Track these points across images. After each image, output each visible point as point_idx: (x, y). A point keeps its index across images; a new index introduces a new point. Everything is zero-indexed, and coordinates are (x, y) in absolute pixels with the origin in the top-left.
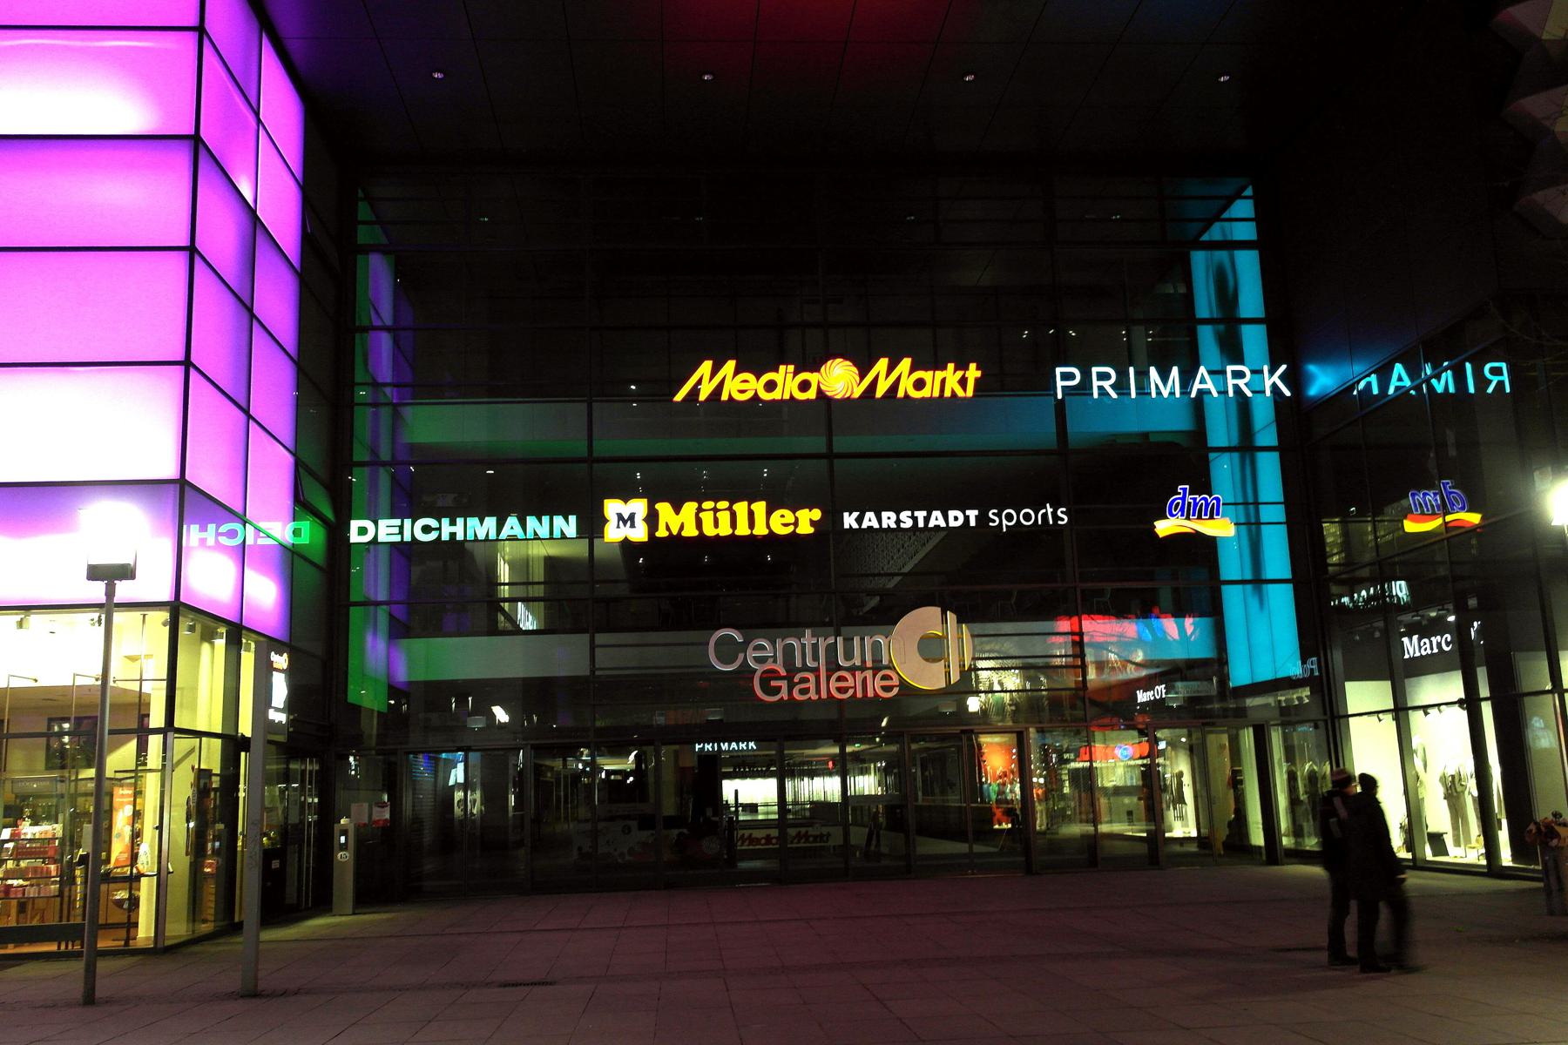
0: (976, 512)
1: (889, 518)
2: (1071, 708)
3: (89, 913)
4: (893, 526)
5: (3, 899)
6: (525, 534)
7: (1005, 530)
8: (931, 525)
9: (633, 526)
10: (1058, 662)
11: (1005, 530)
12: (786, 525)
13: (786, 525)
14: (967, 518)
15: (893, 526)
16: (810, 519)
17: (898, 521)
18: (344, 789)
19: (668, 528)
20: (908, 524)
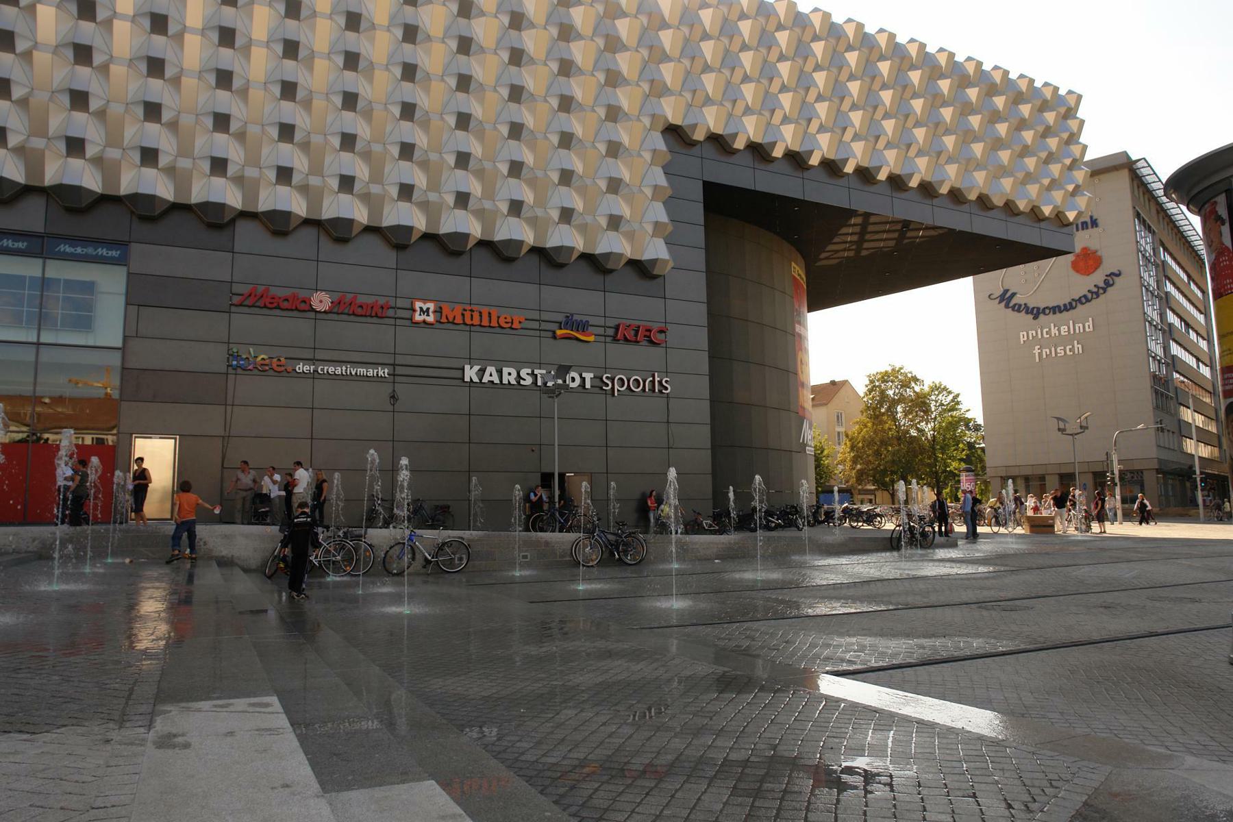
0: (592, 375)
1: (510, 374)
2: (790, 524)
3: (1213, 290)
4: (513, 382)
5: (1231, 176)
6: (490, 322)
7: (57, 250)
8: (485, 380)
9: (428, 315)
10: (943, 528)
11: (57, 250)
12: (506, 322)
13: (506, 322)
14: (583, 379)
15: (513, 382)
16: (697, 124)
17: (519, 377)
18: (798, 609)
19: (447, 318)
20: (528, 381)
